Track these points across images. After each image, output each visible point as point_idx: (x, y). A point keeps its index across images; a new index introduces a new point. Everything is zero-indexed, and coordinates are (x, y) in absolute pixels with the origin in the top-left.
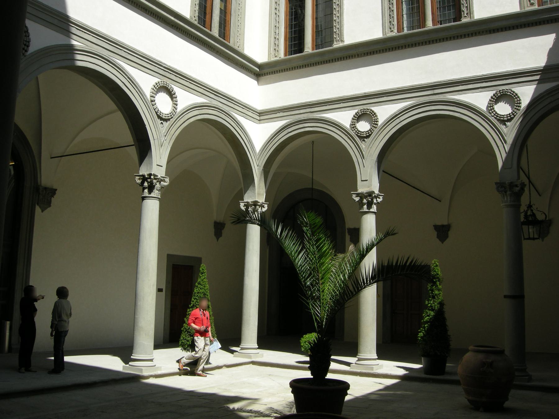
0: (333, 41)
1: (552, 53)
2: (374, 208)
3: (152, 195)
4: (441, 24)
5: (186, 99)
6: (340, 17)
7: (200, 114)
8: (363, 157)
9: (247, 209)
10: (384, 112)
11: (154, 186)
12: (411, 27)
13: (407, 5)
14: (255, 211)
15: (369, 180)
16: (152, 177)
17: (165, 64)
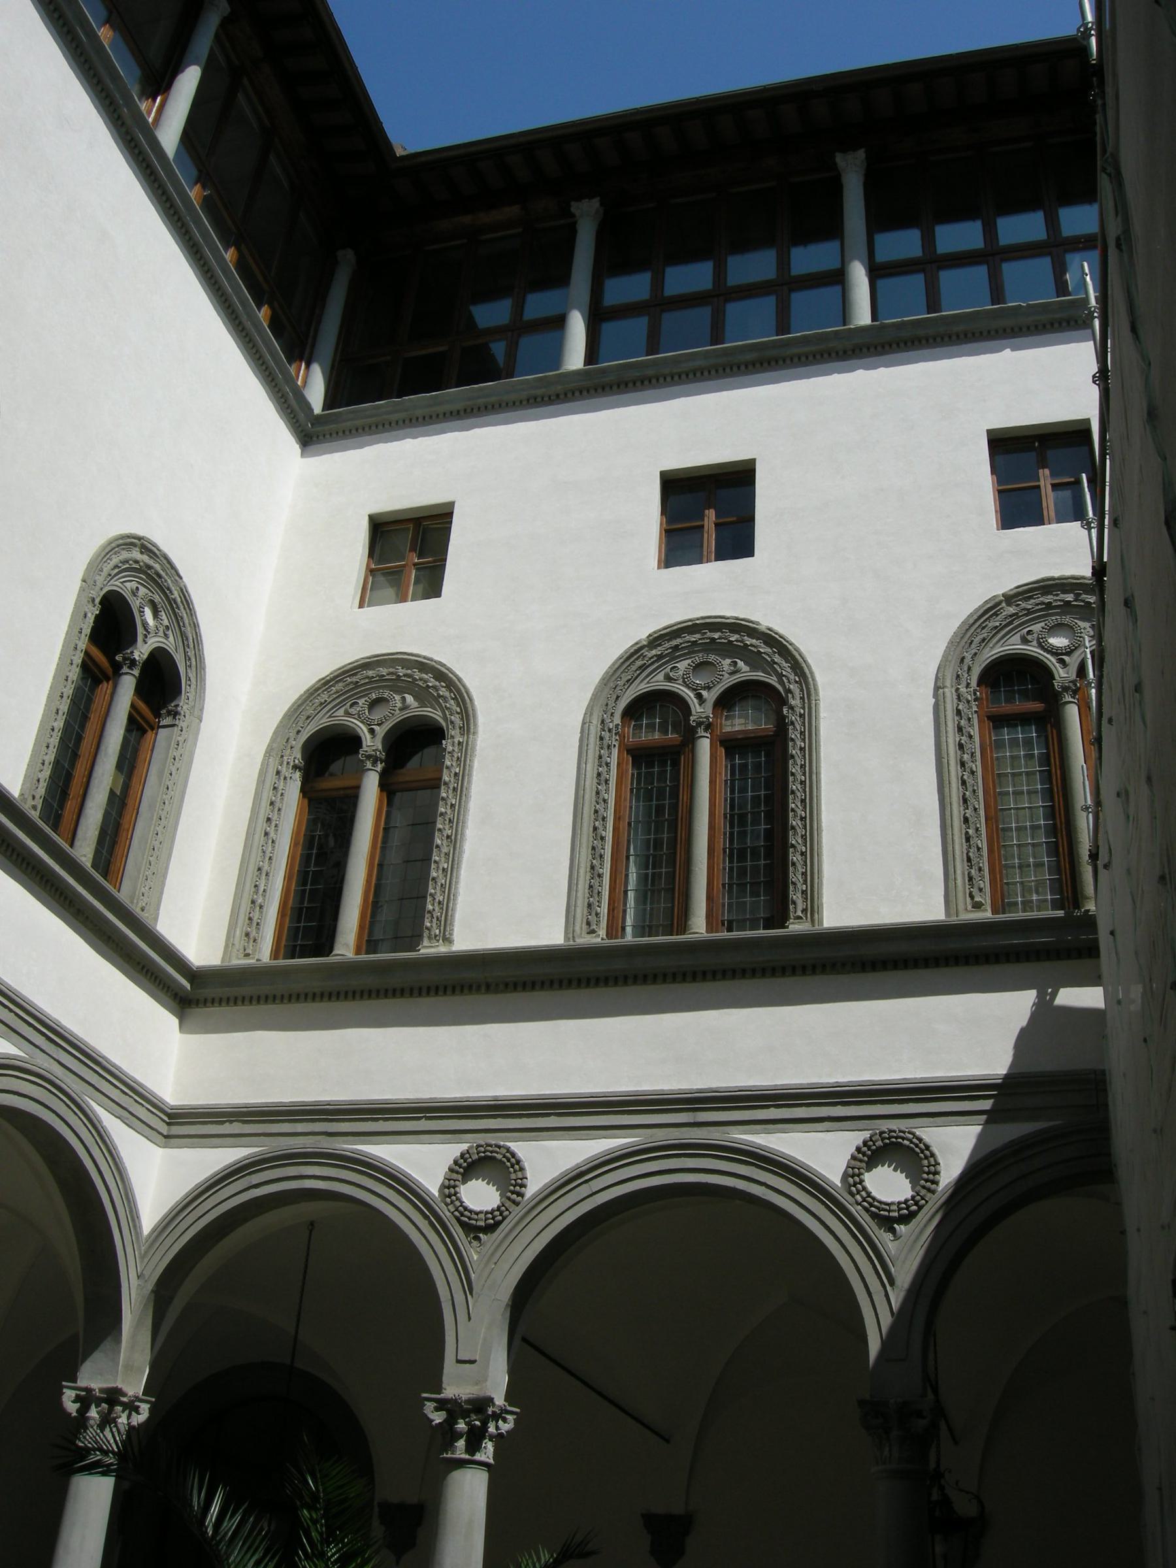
0: (420, 937)
1: (1025, 1041)
2: (487, 1452)
4: (730, 930)
6: (451, 871)
8: (469, 1287)
9: (83, 1410)
10: (546, 1160)
12: (642, 928)
13: (638, 867)
14: (107, 1420)
15: (479, 1362)
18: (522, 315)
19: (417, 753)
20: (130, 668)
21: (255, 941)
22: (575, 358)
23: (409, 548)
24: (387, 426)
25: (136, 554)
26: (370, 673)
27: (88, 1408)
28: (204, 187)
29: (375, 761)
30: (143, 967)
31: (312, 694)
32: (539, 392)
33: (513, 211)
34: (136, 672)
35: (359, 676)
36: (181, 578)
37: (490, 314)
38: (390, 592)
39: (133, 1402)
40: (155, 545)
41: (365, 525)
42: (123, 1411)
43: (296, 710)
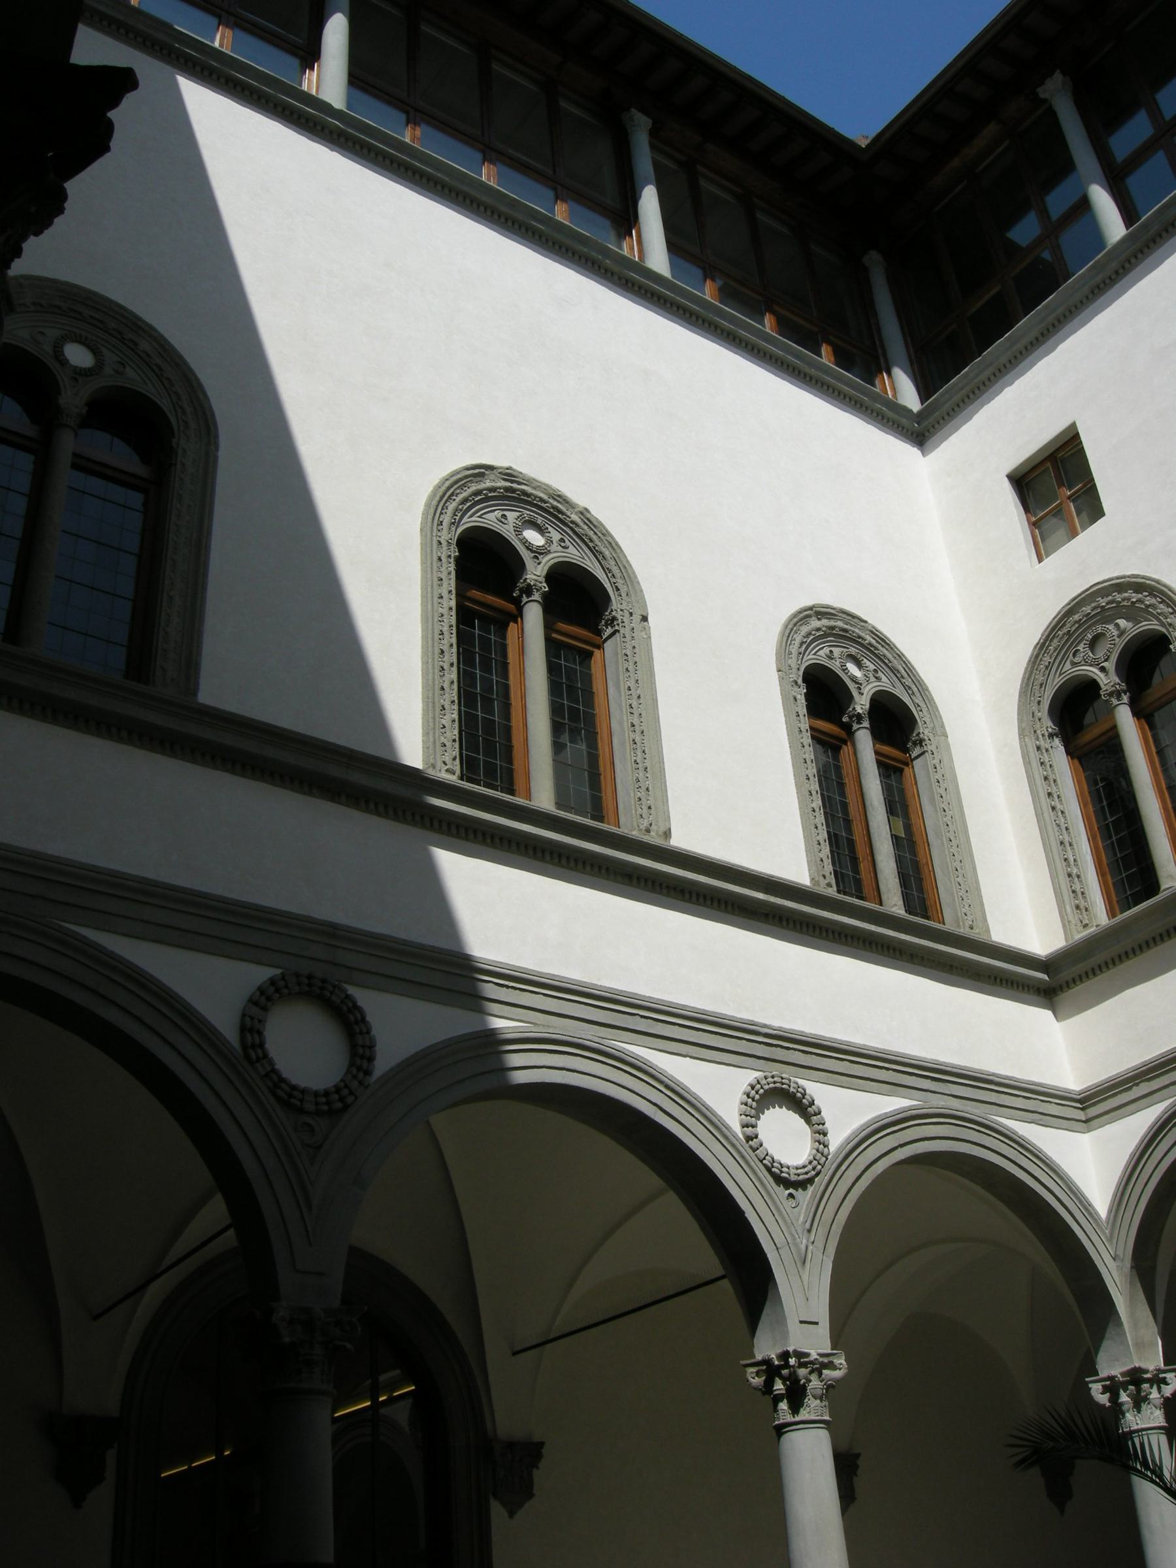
3: (804, 1415)
5: (848, 1110)
7: (902, 1146)
9: (1114, 1398)
11: (804, 1388)
16: (792, 1361)
17: (765, 1026)
18: (1048, 216)
19: (1155, 668)
20: (859, 723)
21: (1086, 910)
22: (1114, 226)
23: (1056, 485)
24: (982, 388)
25: (815, 623)
26: (1076, 617)
27: (1117, 1396)
28: (713, 280)
29: (1118, 694)
30: (995, 978)
31: (1034, 663)
32: (1099, 279)
33: (992, 129)
34: (866, 724)
35: (1068, 625)
36: (866, 622)
37: (1025, 231)
38: (1061, 533)
39: (1157, 1375)
40: (828, 607)
41: (1007, 486)
42: (1151, 1387)
43: (1027, 684)
